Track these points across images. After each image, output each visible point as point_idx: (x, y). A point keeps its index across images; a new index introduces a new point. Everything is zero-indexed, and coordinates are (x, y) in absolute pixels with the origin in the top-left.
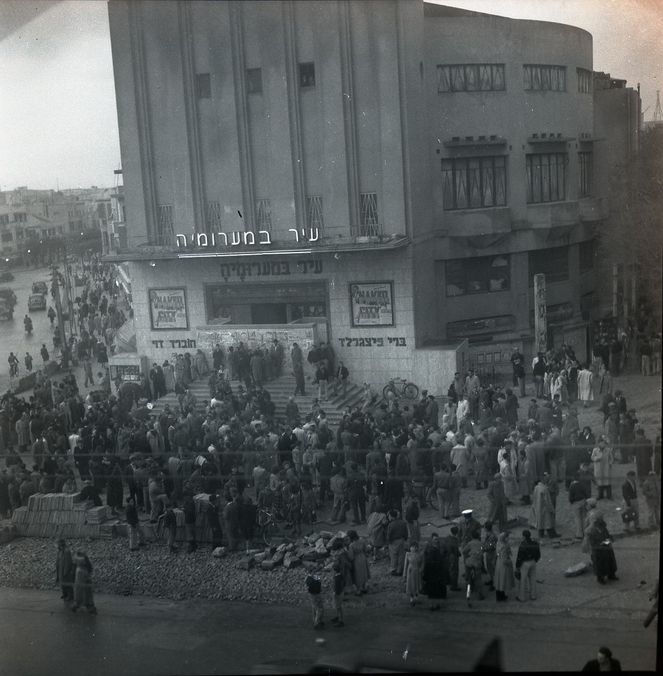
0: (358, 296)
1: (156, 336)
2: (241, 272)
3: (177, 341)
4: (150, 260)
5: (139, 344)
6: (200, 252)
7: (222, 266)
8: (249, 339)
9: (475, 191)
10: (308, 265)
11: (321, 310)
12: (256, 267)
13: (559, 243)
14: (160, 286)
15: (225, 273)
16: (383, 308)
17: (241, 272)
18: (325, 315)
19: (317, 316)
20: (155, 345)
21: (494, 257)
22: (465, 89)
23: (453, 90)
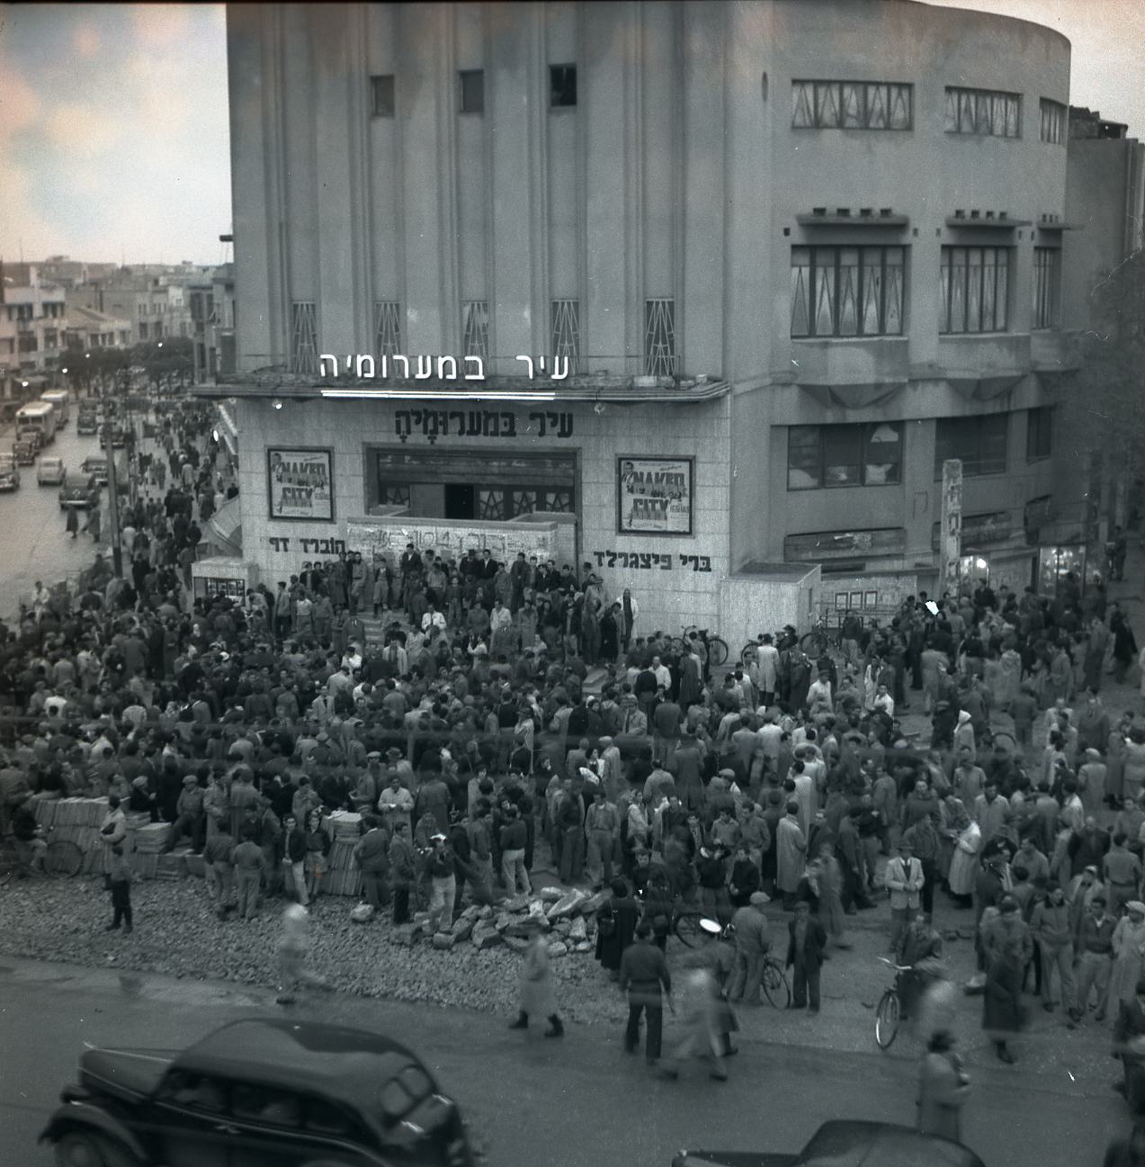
0: (632, 480)
1: (276, 530)
2: (430, 427)
3: (314, 541)
4: (272, 398)
5: (247, 544)
6: (360, 387)
7: (398, 414)
8: (438, 544)
9: (849, 308)
10: (548, 421)
11: (565, 501)
12: (457, 420)
13: (991, 408)
14: (288, 444)
15: (403, 428)
16: (675, 502)
17: (430, 427)
18: (572, 510)
19: (557, 510)
20: (273, 547)
21: (875, 426)
22: (840, 124)
23: (818, 124)
